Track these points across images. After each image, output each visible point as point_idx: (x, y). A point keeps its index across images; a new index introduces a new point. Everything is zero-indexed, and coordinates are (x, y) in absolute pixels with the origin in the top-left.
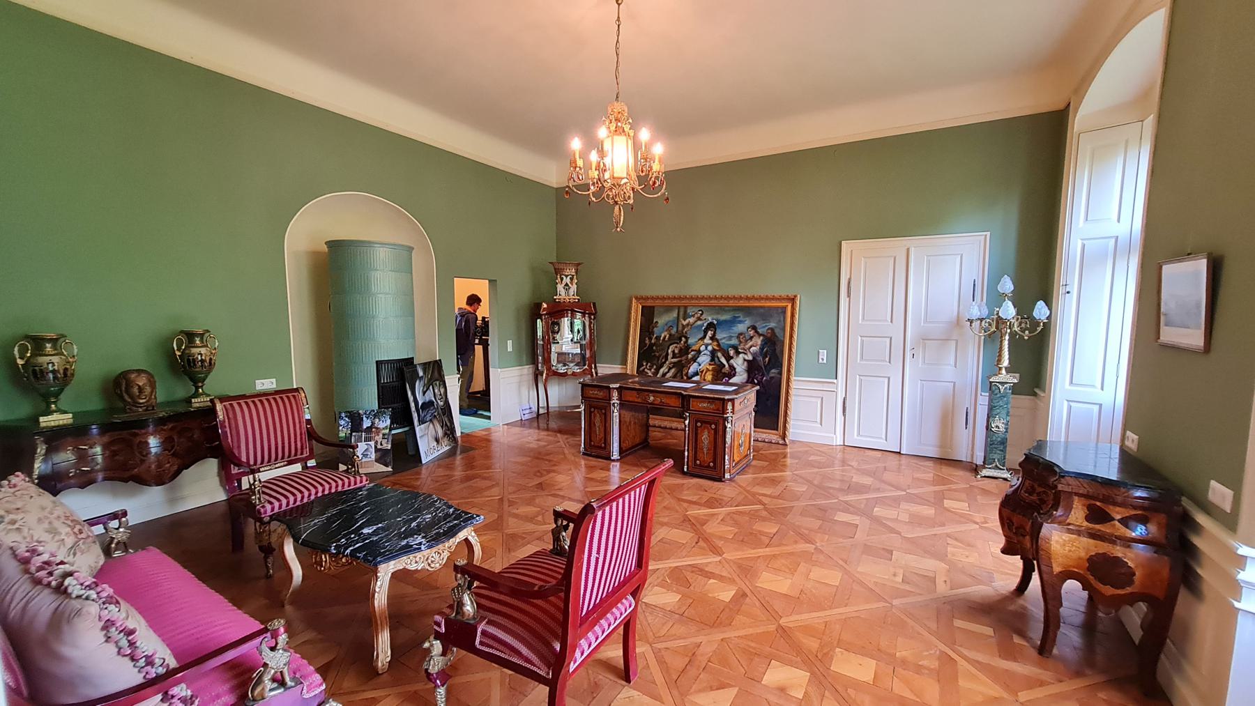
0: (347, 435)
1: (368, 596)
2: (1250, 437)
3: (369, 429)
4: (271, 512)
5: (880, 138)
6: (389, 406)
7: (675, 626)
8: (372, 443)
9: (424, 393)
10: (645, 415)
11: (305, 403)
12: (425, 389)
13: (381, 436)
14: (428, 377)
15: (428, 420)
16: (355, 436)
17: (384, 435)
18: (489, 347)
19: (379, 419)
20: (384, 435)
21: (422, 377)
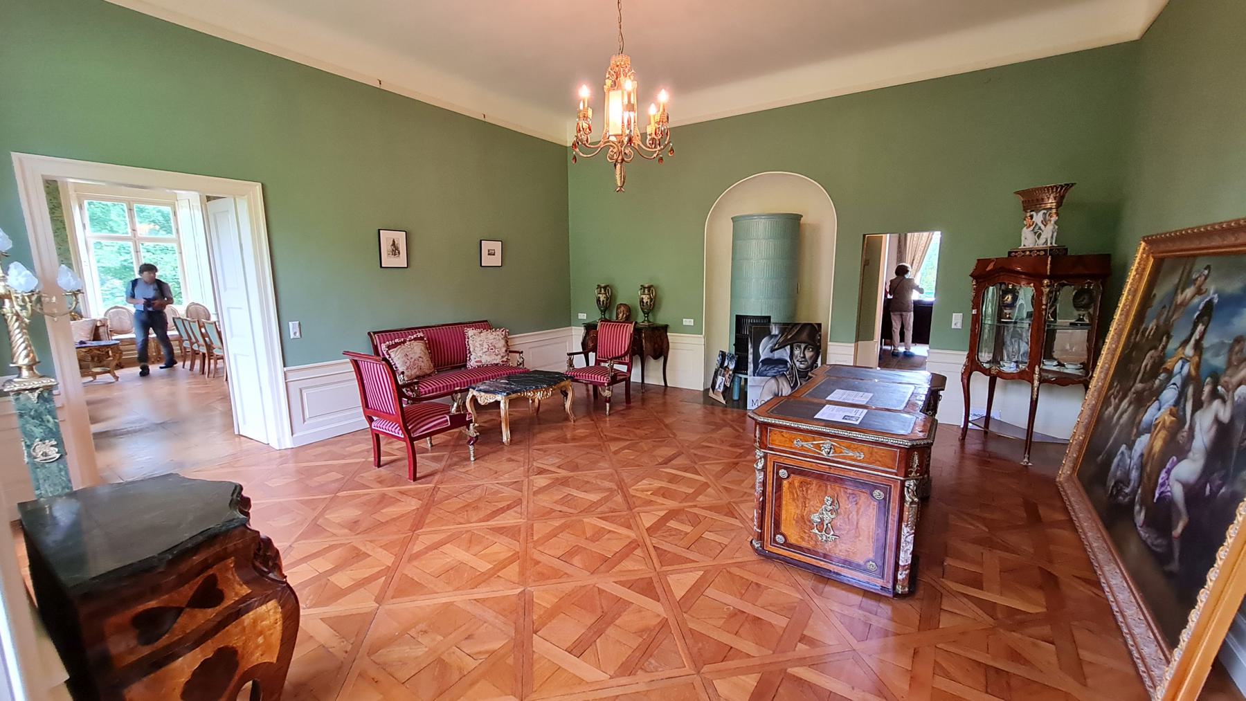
9: (772, 350)
10: (668, 385)
12: (777, 346)
14: (787, 336)
21: (776, 336)
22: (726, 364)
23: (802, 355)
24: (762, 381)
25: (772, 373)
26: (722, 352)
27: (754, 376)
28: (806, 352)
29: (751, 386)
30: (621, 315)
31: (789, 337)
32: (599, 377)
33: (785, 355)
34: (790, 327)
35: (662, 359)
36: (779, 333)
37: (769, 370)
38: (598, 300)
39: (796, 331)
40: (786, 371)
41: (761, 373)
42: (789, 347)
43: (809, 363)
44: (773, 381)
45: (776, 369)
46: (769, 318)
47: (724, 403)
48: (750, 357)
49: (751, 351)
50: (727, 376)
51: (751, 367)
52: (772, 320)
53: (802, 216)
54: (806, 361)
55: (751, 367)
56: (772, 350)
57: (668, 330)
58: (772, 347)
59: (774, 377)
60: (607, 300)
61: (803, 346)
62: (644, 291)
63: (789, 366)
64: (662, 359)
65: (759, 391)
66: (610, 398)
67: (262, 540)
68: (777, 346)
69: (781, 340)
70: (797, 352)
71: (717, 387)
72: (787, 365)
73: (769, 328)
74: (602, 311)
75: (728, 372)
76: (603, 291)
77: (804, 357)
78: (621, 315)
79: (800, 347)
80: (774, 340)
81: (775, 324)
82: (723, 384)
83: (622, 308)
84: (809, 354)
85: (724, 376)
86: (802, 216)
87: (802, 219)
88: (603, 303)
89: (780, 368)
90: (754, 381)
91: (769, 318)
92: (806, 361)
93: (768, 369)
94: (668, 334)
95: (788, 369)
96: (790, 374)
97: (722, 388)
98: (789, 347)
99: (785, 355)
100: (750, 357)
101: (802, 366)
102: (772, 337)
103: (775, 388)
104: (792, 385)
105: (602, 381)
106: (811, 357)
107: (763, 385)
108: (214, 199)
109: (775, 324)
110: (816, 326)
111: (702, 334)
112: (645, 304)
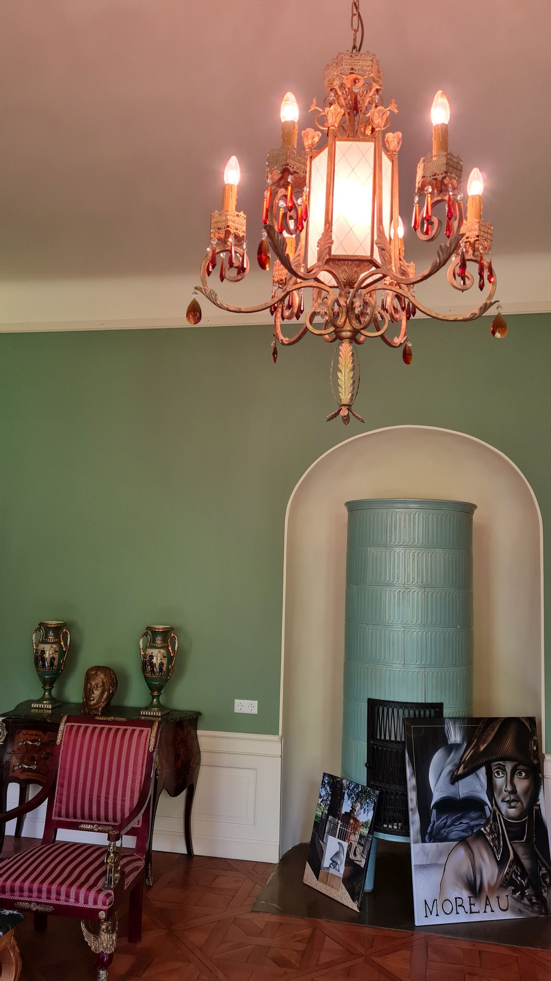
0: (323, 817)
1: (415, 191)
2: (190, 303)
3: (349, 815)
4: (88, 727)
5: (545, 654)
6: (377, 784)
7: (122, 852)
8: (345, 844)
9: (455, 779)
10: (197, 851)
11: (462, 727)
12: (461, 771)
13: (357, 837)
14: (477, 746)
15: (453, 835)
16: (330, 822)
17: (361, 836)
18: (366, 761)
19: (361, 804)
20: (361, 836)
21: (456, 746)
22: (346, 808)
23: (509, 788)
24: (440, 854)
25: (456, 831)
26: (330, 776)
27: (423, 841)
28: (516, 781)
29: (423, 867)
30: (97, 693)
31: (482, 748)
32: (83, 891)
33: (478, 787)
34: (481, 725)
35: (183, 795)
36: (463, 740)
37: (452, 824)
38: (39, 658)
39: (493, 734)
40: (485, 826)
41: (438, 833)
42: (483, 769)
43: (525, 805)
44: (461, 852)
45: (464, 821)
46: (439, 707)
47: (356, 909)
48: (412, 796)
49: (411, 782)
50: (354, 838)
51: (415, 819)
52: (447, 712)
53: (474, 507)
54: (518, 800)
55: (415, 819)
56: (455, 779)
57: (199, 724)
58: (452, 773)
59: (463, 841)
60: (61, 657)
61: (509, 767)
62: (154, 641)
63: (488, 813)
64: (183, 795)
65: (435, 876)
66: (111, 956)
67: (432, 222)
68: (461, 771)
69: (468, 756)
70: (499, 781)
71: (326, 863)
72: (484, 811)
73: (443, 728)
74: (44, 682)
75: (355, 829)
76: (51, 638)
77: (514, 791)
78: (97, 693)
79: (504, 770)
80: (455, 757)
81: (454, 719)
82: (343, 857)
83: (101, 678)
84: (521, 784)
85: (343, 836)
86: (474, 507)
87: (476, 512)
88: (52, 664)
89: (472, 819)
90: (426, 854)
91: (439, 707)
92: (518, 800)
93: (449, 822)
94: (199, 732)
95: (488, 820)
96: (491, 832)
97: (342, 868)
98: (483, 769)
99: (478, 787)
100: (412, 796)
101: (512, 812)
102: (451, 748)
103: (466, 867)
104: (499, 857)
105: (90, 905)
106: (526, 792)
107: (443, 861)
108: (515, 851)
109: (454, 719)
110: (527, 724)
111: (276, 733)
112: (157, 669)
